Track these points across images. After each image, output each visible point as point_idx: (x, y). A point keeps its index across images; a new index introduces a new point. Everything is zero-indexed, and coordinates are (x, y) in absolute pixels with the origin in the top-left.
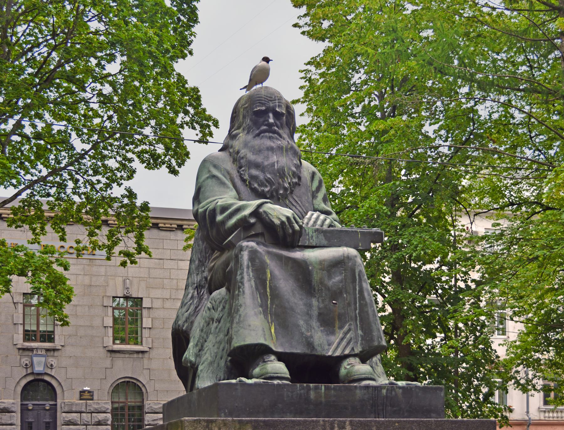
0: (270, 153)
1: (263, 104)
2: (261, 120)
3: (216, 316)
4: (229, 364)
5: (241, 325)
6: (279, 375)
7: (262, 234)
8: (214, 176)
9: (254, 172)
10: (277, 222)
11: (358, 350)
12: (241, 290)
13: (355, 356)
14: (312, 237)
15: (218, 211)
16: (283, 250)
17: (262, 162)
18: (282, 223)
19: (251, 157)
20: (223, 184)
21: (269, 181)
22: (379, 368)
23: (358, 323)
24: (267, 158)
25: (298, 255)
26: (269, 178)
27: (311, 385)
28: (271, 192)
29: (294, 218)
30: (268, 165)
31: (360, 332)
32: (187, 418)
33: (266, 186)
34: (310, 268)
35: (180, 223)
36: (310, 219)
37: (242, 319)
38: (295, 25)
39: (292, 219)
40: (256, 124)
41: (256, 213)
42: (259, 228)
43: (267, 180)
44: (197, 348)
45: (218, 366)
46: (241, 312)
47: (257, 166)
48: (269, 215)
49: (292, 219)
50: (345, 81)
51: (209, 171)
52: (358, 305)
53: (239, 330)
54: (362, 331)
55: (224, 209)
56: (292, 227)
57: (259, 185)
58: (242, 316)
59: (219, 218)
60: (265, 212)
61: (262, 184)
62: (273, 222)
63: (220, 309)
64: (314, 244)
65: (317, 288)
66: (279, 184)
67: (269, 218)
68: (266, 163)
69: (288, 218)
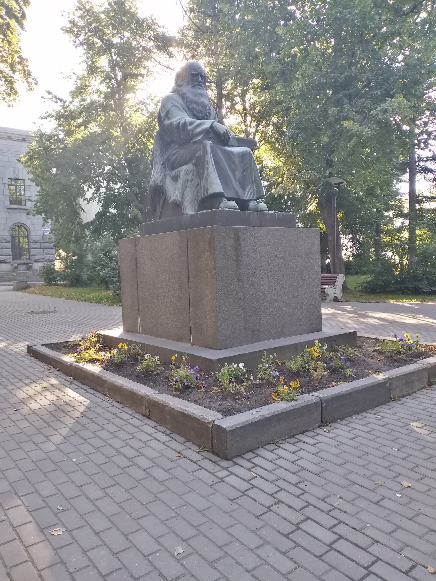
1: (197, 71)
2: (195, 79)
3: (190, 178)
7: (213, 137)
8: (175, 106)
9: (195, 106)
10: (222, 132)
11: (255, 198)
15: (188, 124)
19: (193, 98)
25: (228, 148)
31: (255, 189)
32: (381, 377)
38: (43, 97)
40: (193, 81)
47: (196, 103)
50: (384, 29)
51: (172, 103)
59: (190, 128)
63: (191, 175)
68: (199, 102)
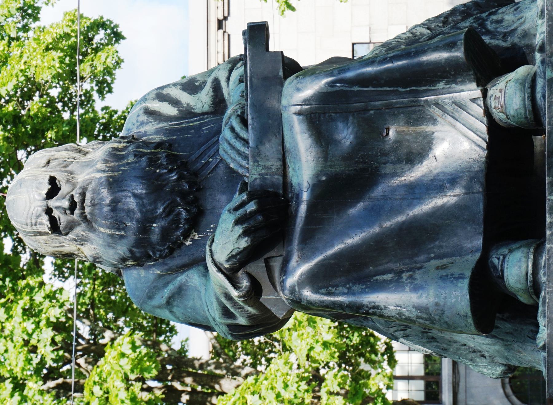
0: (120, 205)
4: (506, 315)
5: (437, 318)
6: (530, 271)
12: (371, 311)
13: (485, 94)
14: (266, 167)
15: (230, 321)
16: (294, 225)
17: (137, 221)
18: (245, 233)
20: (180, 291)
21: (169, 211)
22: (507, 17)
23: (424, 88)
24: (129, 212)
26: (164, 211)
27: (548, 220)
28: (187, 204)
29: (236, 209)
30: (141, 212)
33: (179, 214)
34: (324, 178)
35: (214, 25)
36: (234, 160)
37: (425, 316)
39: (240, 212)
41: (231, 276)
42: (257, 268)
43: (168, 215)
44: (478, 360)
45: (512, 333)
46: (411, 315)
48: (234, 253)
49: (240, 212)
52: (388, 89)
53: (446, 322)
54: (439, 81)
55: (226, 313)
56: (252, 214)
57: (177, 228)
58: (420, 314)
59: (242, 321)
60: (228, 260)
61: (176, 222)
62: (245, 249)
64: (279, 164)
65: (361, 166)
66: (172, 191)
67: (237, 254)
69: (238, 222)
